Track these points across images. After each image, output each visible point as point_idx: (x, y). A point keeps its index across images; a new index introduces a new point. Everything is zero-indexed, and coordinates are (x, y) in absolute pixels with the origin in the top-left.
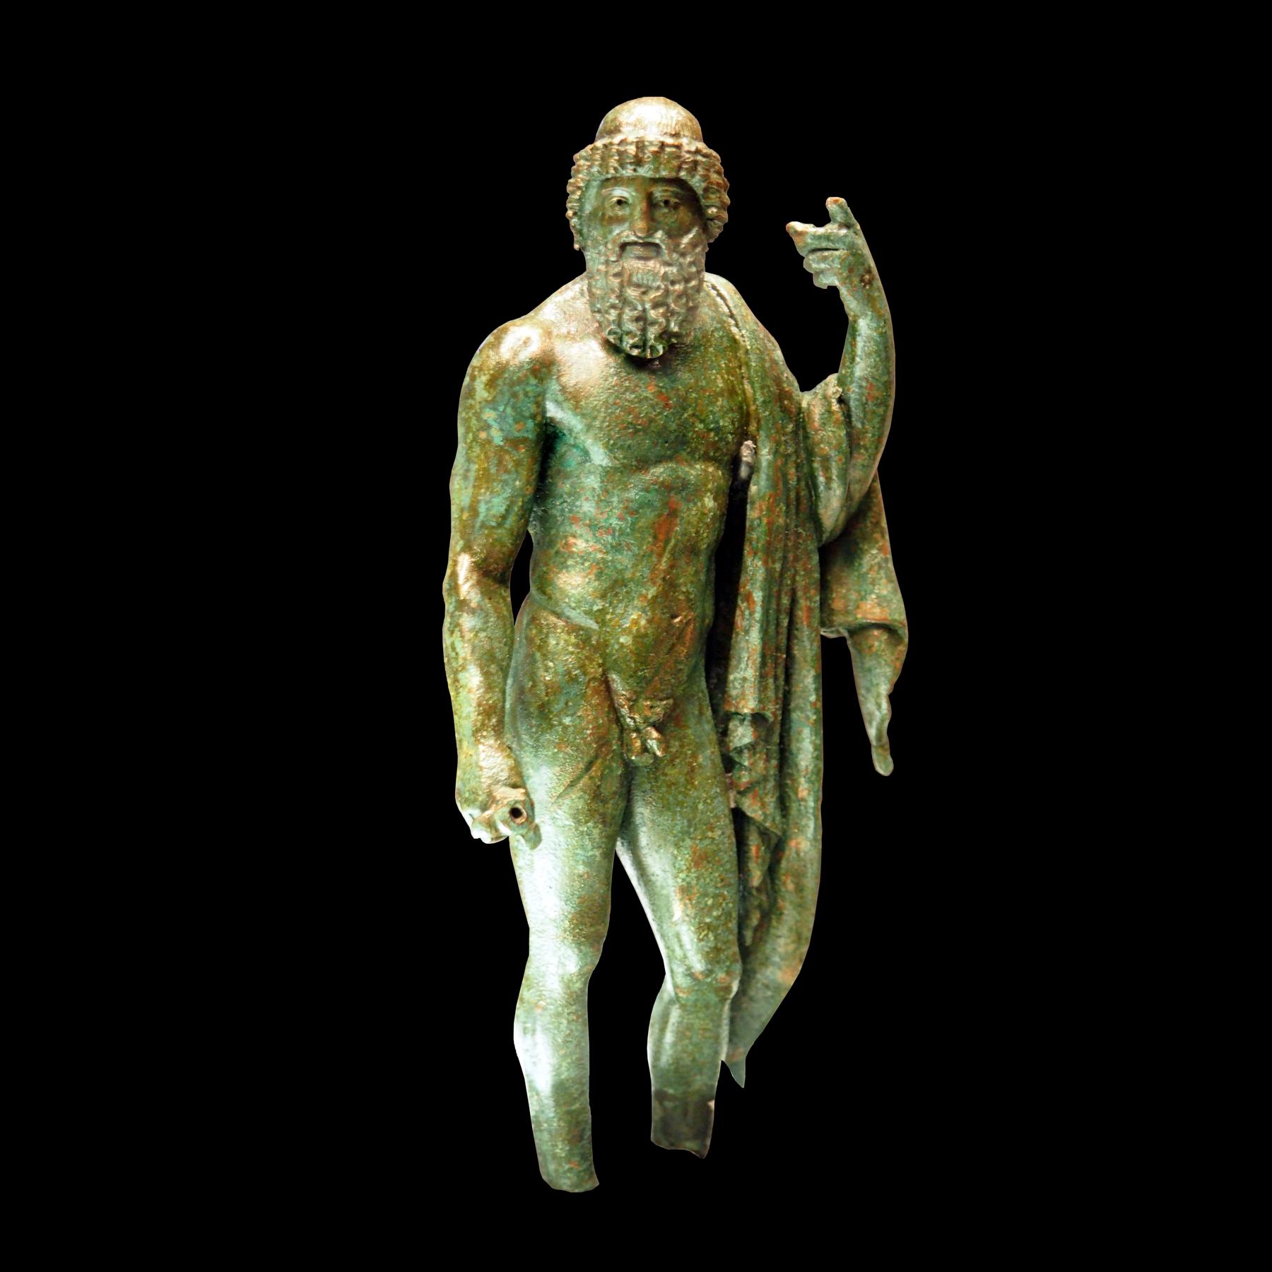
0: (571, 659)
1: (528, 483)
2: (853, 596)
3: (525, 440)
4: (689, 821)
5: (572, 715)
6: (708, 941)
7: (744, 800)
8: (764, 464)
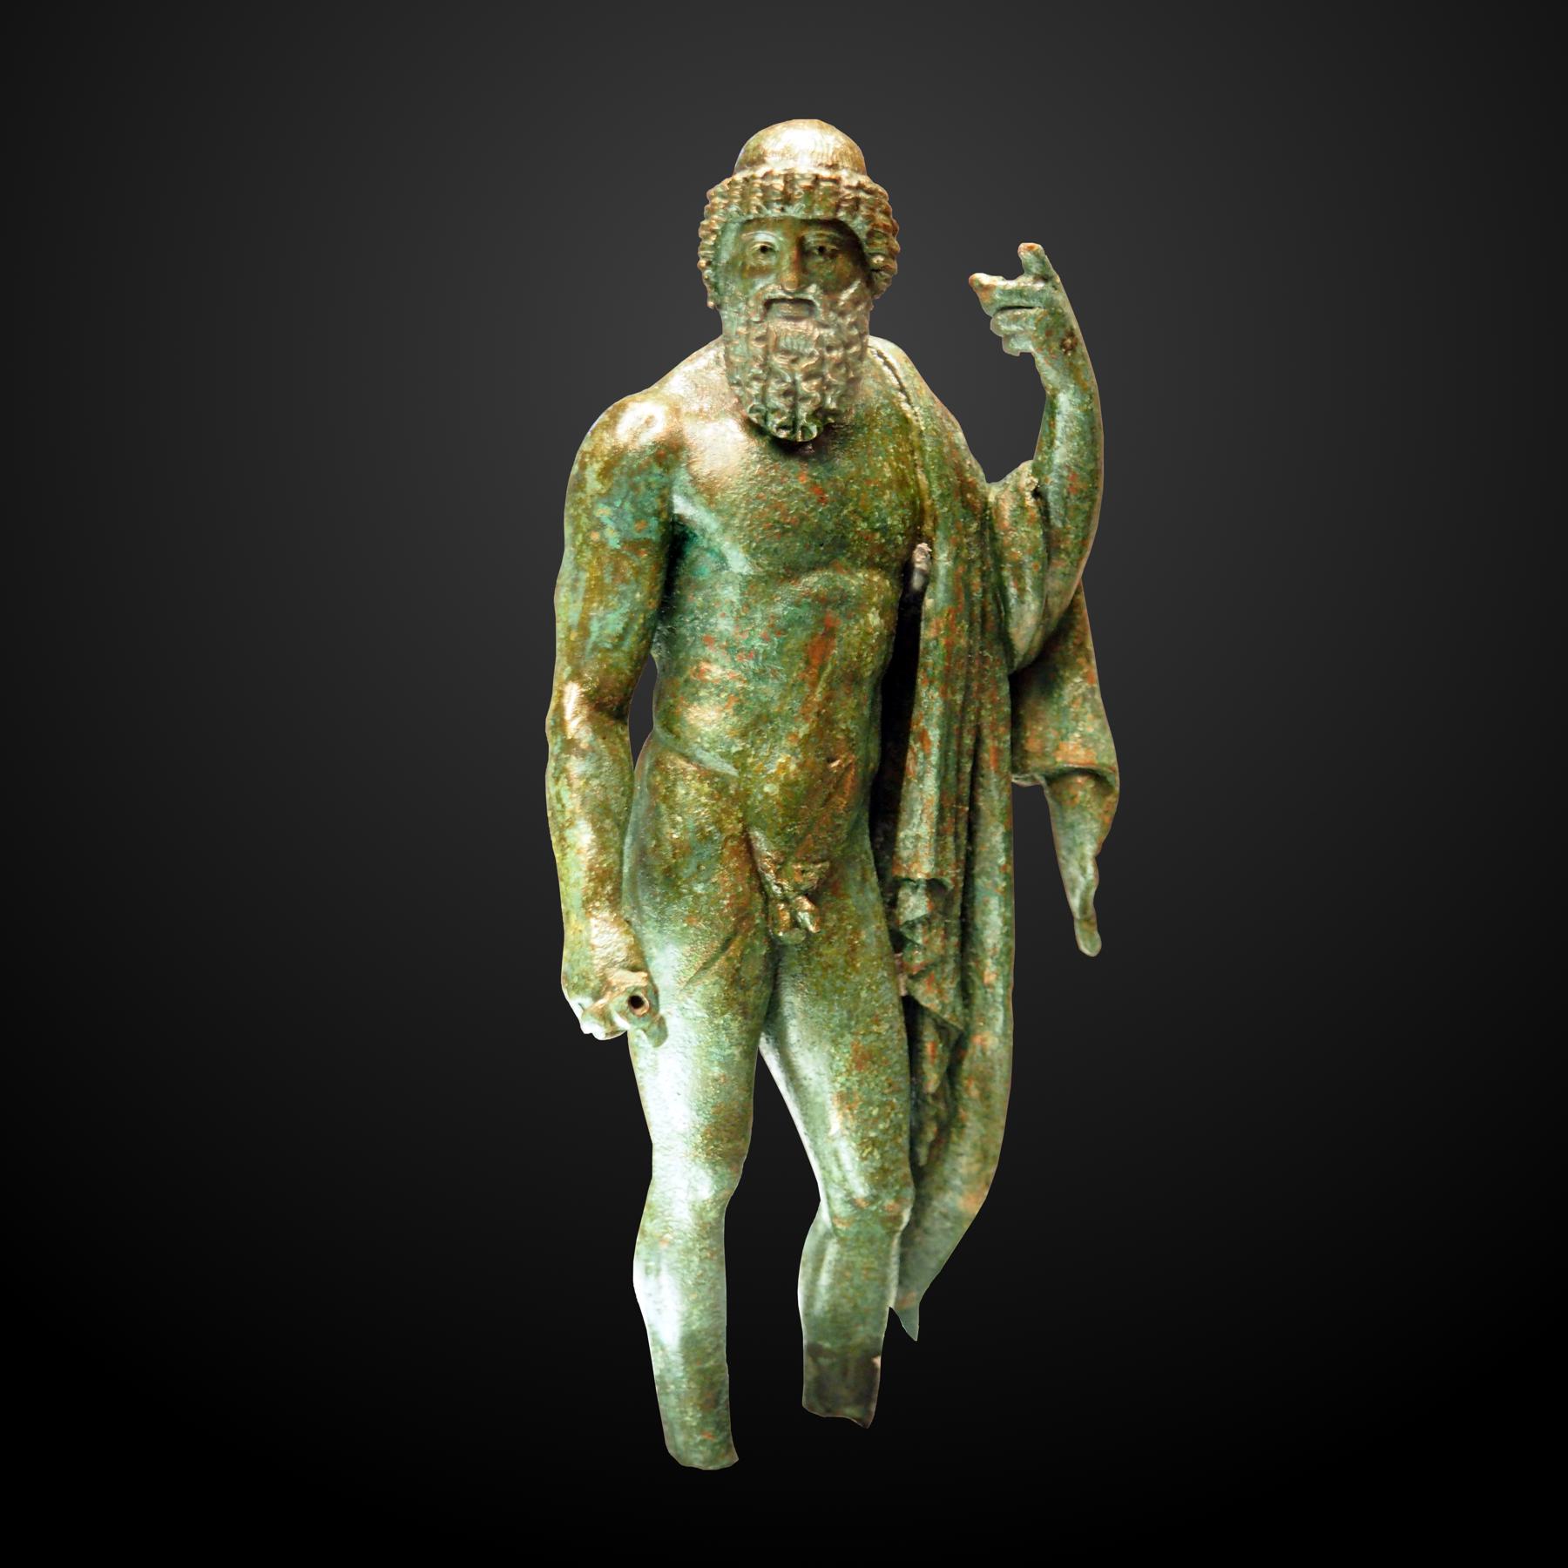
0: (703, 812)
1: (651, 595)
2: (1052, 735)
3: (647, 542)
4: (849, 1012)
5: (705, 882)
6: (873, 1160)
7: (917, 986)
8: (942, 572)
